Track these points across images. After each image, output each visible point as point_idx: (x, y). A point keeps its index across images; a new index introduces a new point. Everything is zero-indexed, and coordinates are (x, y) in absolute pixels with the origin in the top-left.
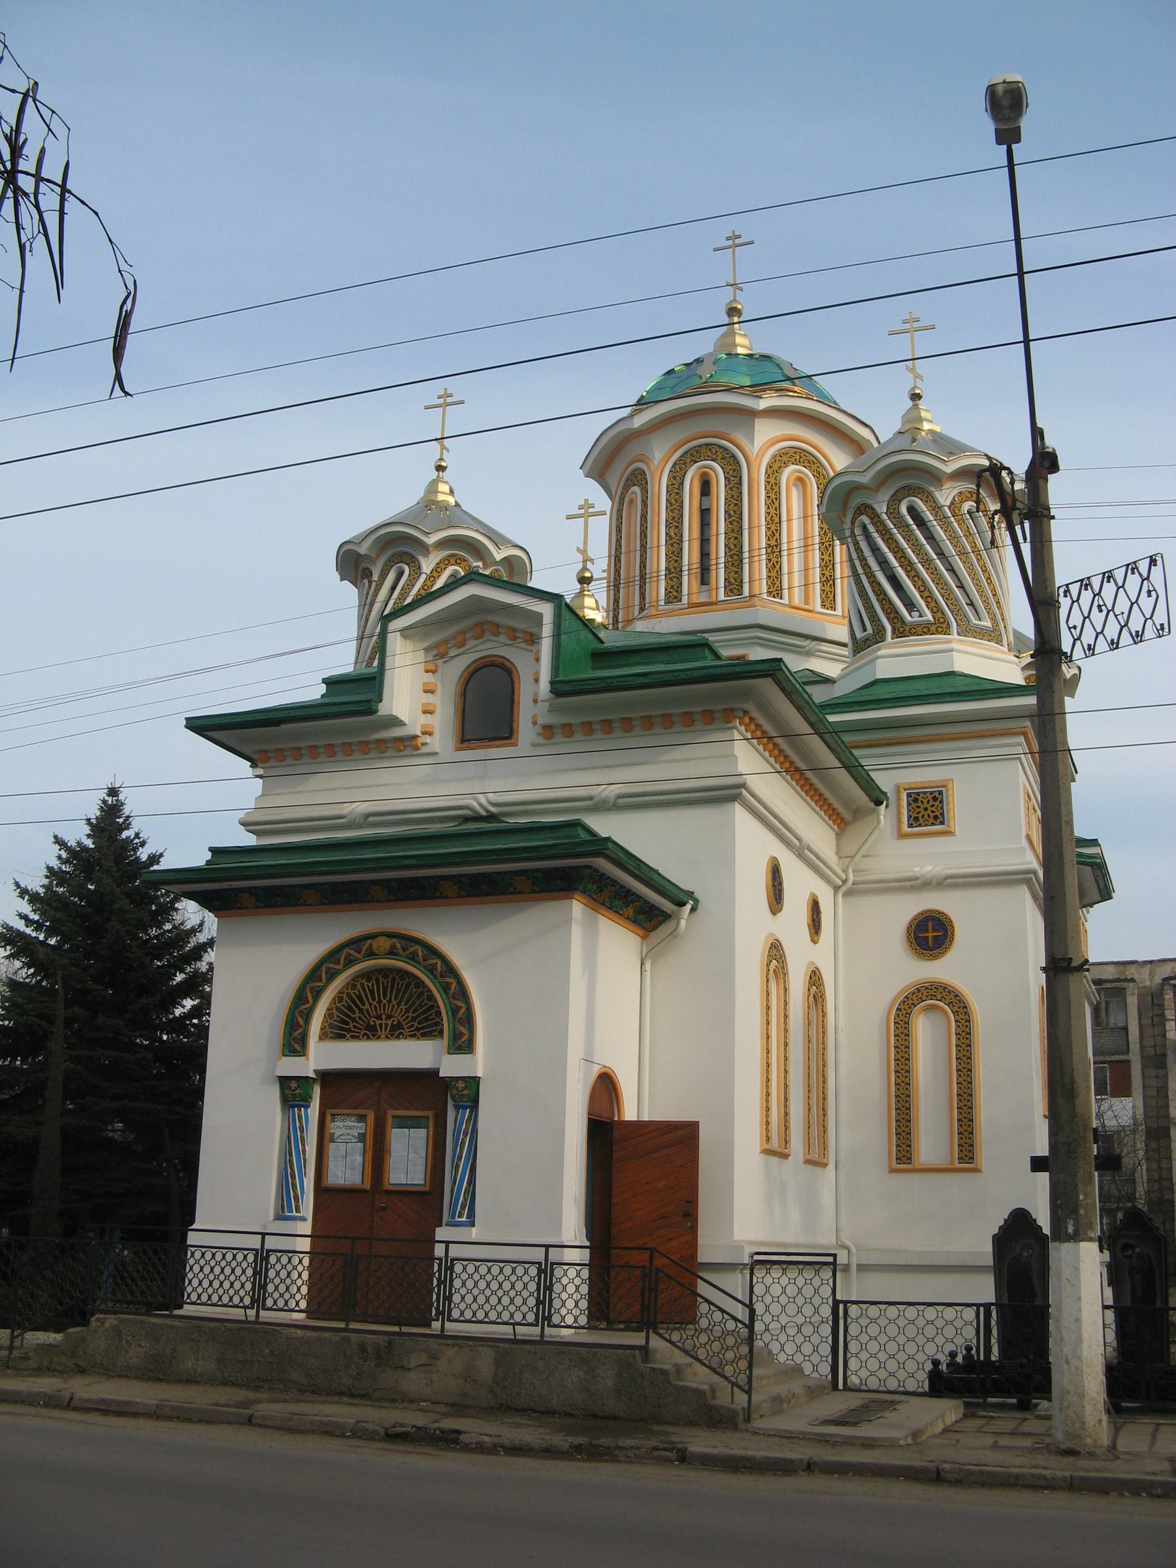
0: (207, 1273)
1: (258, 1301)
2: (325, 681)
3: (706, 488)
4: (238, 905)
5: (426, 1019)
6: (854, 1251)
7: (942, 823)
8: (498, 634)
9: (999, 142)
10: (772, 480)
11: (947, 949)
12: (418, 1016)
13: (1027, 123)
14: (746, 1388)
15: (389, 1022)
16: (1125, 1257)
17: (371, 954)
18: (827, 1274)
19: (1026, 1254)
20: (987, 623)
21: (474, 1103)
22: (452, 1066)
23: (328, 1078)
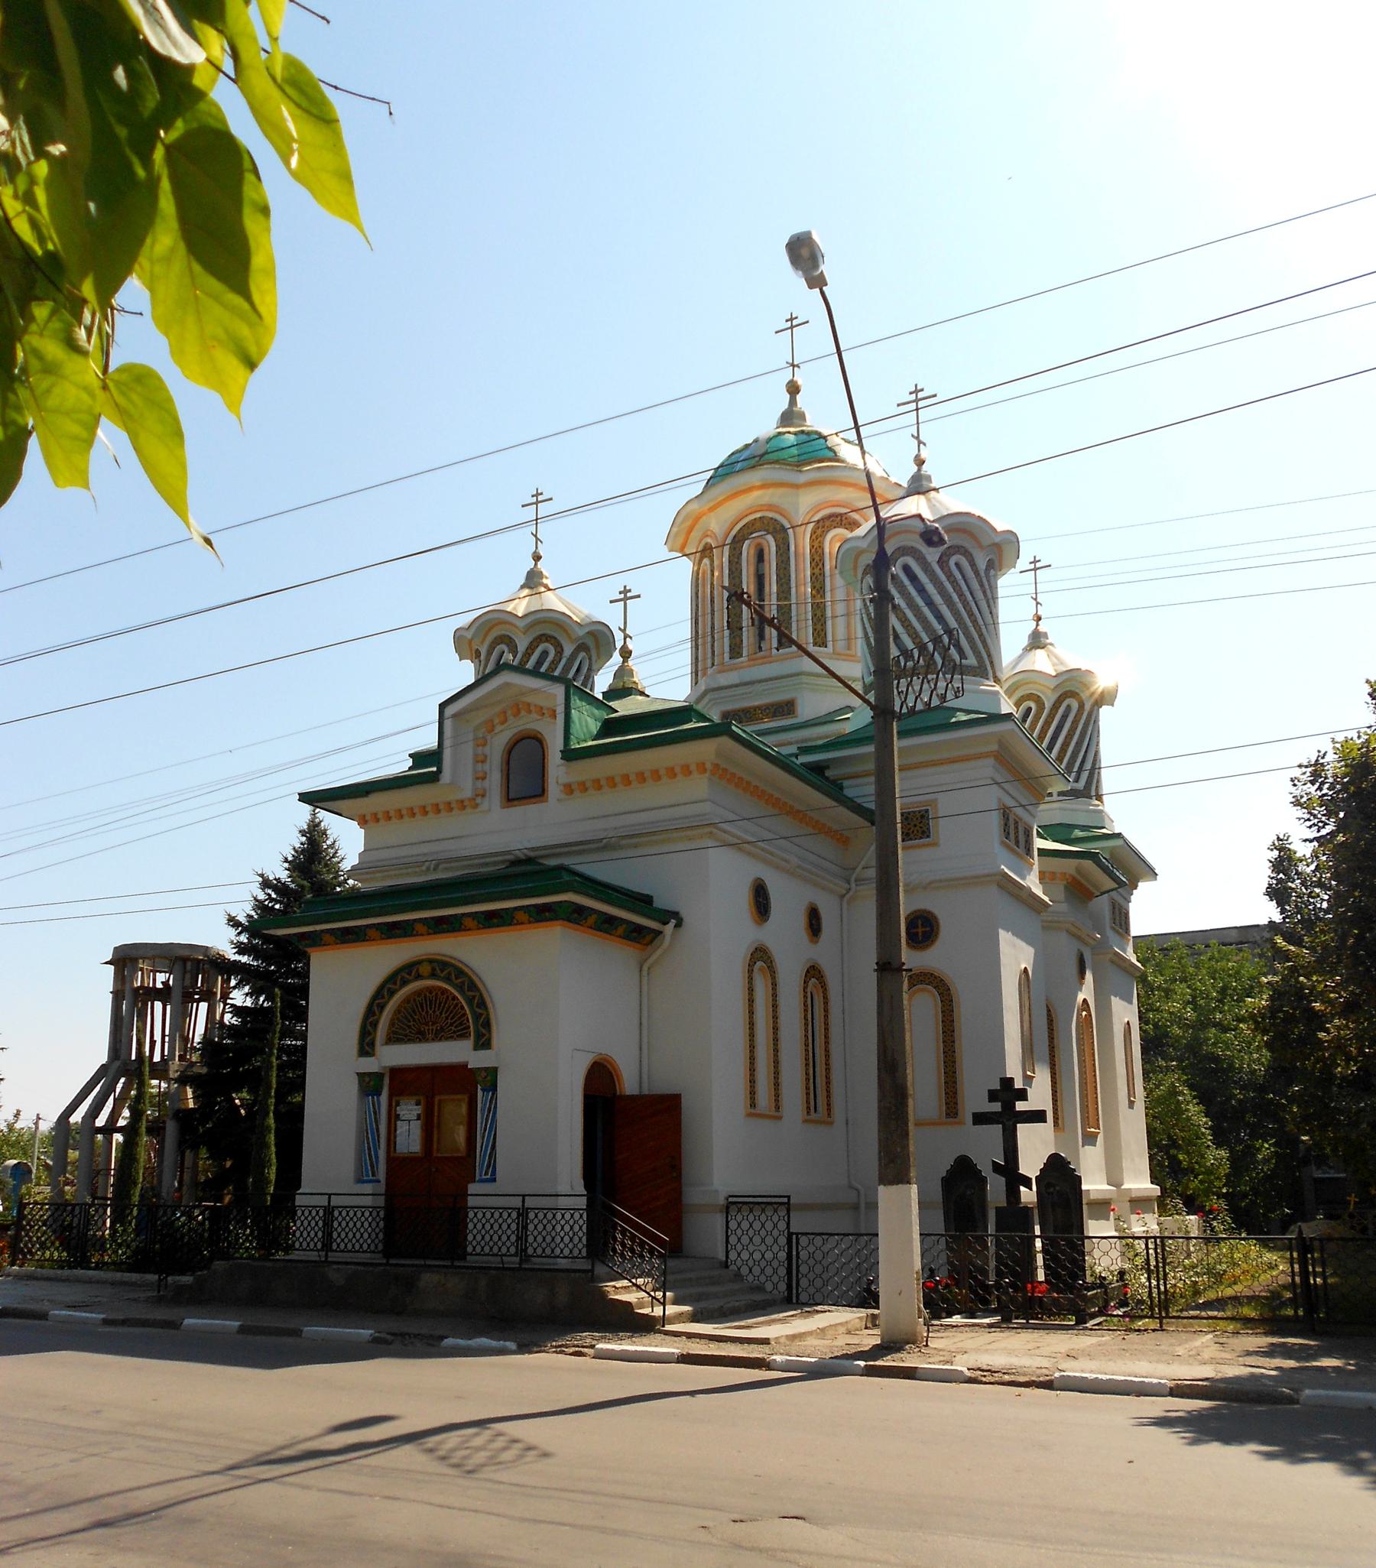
0: (575, 1249)
1: (327, 1246)
2: (410, 755)
3: (760, 556)
4: (323, 943)
5: (461, 1024)
6: (862, 1192)
7: (928, 836)
8: (530, 712)
9: (811, 287)
10: (816, 544)
11: (933, 942)
12: (454, 1022)
13: (826, 268)
14: (662, 1301)
15: (434, 1028)
16: (1049, 1194)
17: (419, 977)
18: (783, 1212)
19: (969, 1193)
20: (972, 661)
21: (493, 1088)
22: (477, 1060)
23: (396, 1072)
